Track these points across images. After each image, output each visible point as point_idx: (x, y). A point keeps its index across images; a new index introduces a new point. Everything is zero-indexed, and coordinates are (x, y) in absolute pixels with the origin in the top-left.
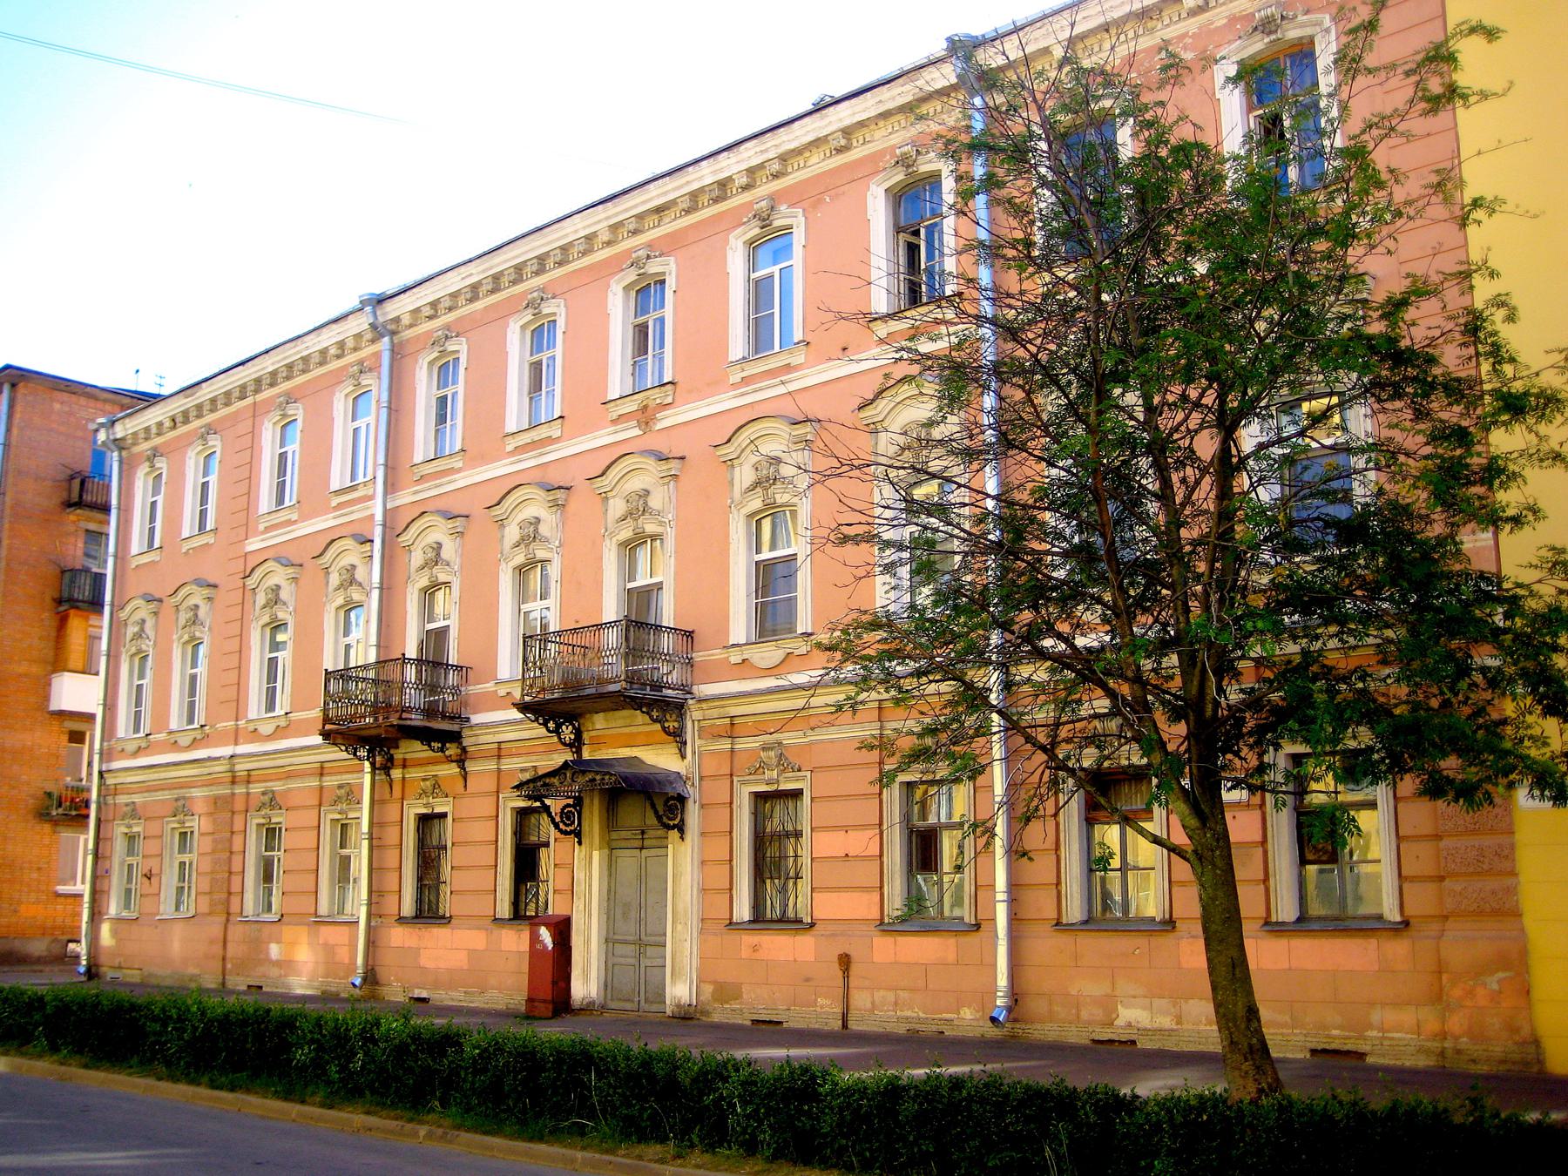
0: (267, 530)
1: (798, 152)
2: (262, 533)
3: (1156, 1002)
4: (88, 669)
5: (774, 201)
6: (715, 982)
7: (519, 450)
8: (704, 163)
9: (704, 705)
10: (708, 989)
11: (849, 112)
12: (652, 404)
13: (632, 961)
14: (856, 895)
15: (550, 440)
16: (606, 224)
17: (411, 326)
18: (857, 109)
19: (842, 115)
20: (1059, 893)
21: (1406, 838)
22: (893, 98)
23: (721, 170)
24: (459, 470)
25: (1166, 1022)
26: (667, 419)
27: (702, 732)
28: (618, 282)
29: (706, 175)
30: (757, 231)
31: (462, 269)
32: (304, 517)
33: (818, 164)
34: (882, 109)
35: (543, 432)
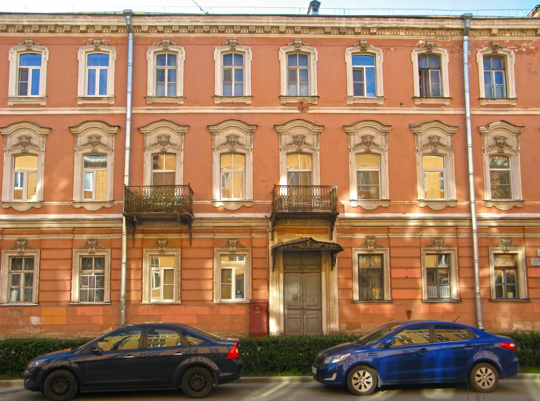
0: (15, 106)
1: (383, 28)
2: (10, 107)
3: (526, 323)
4: (493, 197)
5: (370, 41)
6: (347, 323)
7: (222, 104)
8: (344, 19)
9: (342, 221)
10: (344, 325)
11: (413, 23)
12: (305, 102)
13: (299, 316)
14: (411, 291)
15: (244, 104)
16: (285, 25)
17: (147, 32)
18: (417, 23)
19: (410, 23)
20: (142, 283)
21: (43, 259)
22: (432, 25)
23: (351, 23)
24: (181, 105)
25: (529, 328)
26: (312, 110)
27: (339, 231)
28: (284, 49)
29: (343, 23)
30: (359, 51)
31: (193, 17)
32: (50, 105)
33: (387, 35)
34: (426, 26)
35: (241, 100)
